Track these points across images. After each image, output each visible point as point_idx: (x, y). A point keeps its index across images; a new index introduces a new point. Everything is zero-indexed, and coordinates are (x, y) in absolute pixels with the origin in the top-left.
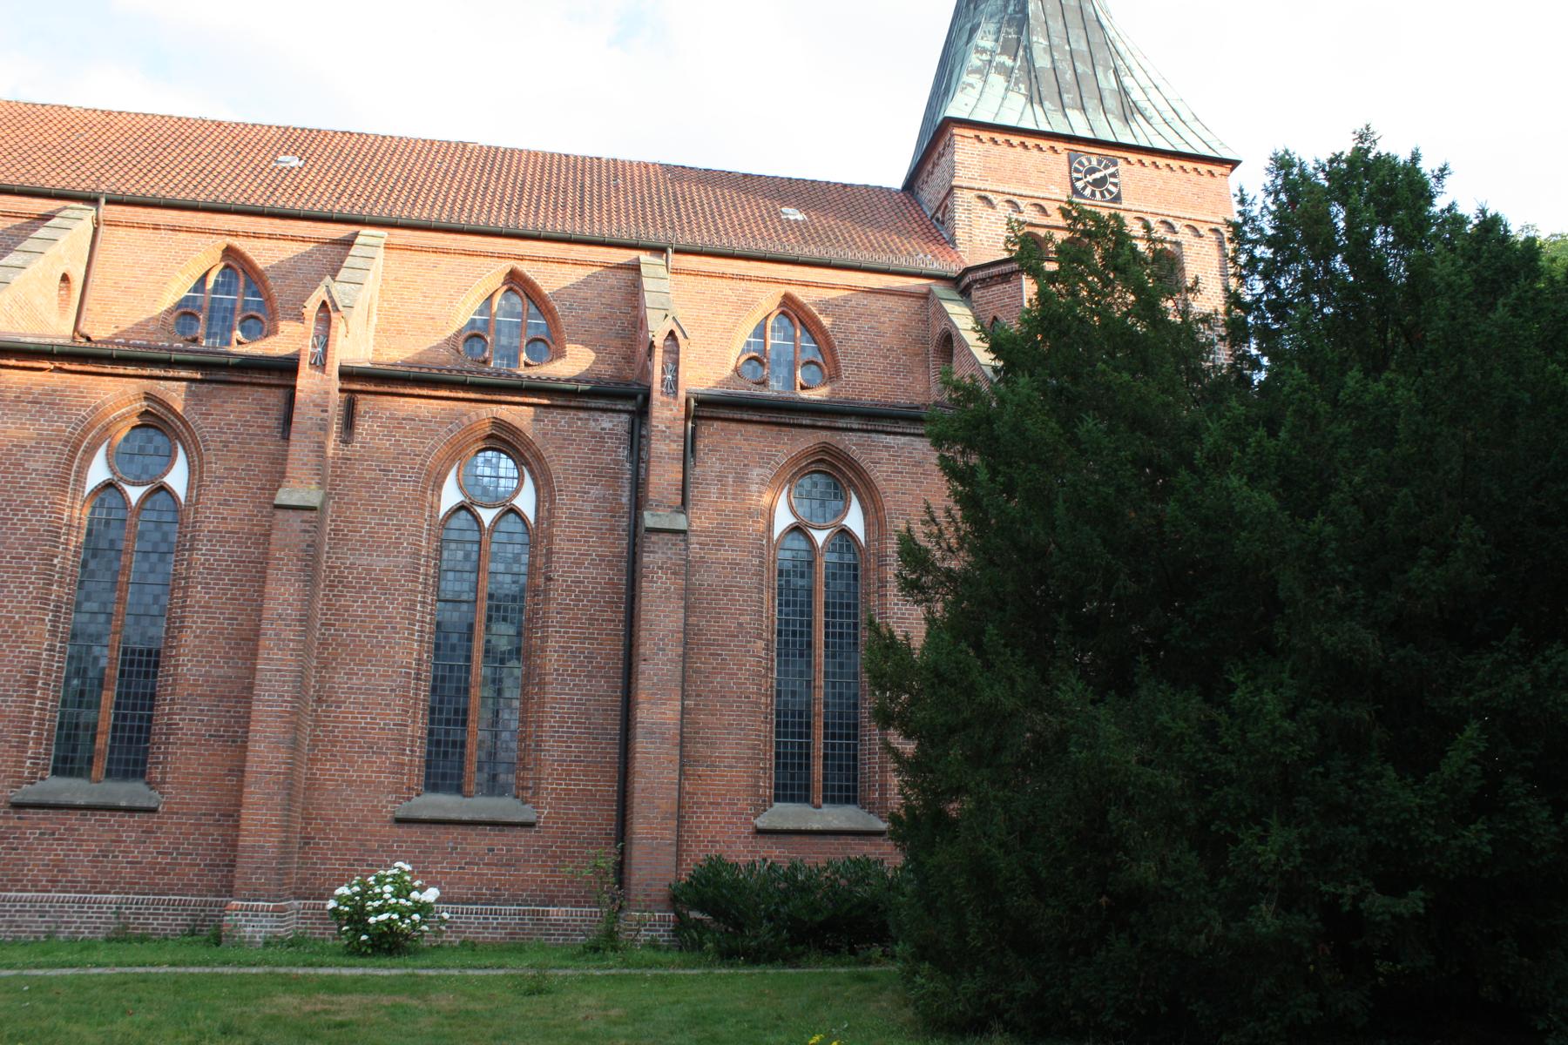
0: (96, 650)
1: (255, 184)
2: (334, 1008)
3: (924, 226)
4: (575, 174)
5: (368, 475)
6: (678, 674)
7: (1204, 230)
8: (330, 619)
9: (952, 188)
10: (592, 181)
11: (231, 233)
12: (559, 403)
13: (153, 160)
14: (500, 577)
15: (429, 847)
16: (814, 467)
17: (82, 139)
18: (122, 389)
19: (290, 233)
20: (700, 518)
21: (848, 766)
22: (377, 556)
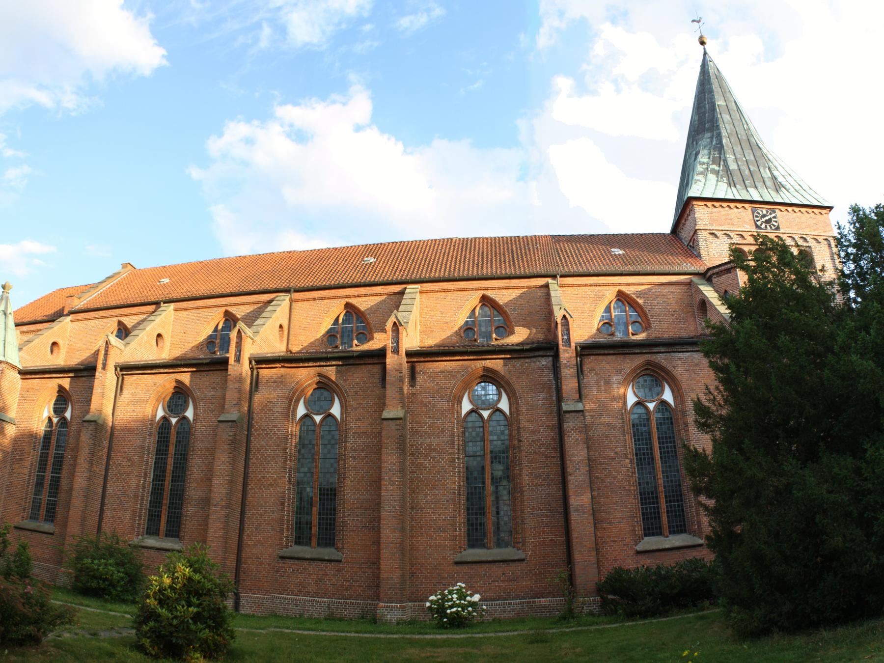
0: (308, 489)
1: (355, 273)
4: (508, 245)
5: (425, 400)
6: (588, 481)
7: (821, 239)
9: (696, 231)
11: (347, 297)
12: (515, 356)
14: (495, 443)
16: (644, 373)
18: (307, 373)
19: (374, 292)
21: (680, 515)
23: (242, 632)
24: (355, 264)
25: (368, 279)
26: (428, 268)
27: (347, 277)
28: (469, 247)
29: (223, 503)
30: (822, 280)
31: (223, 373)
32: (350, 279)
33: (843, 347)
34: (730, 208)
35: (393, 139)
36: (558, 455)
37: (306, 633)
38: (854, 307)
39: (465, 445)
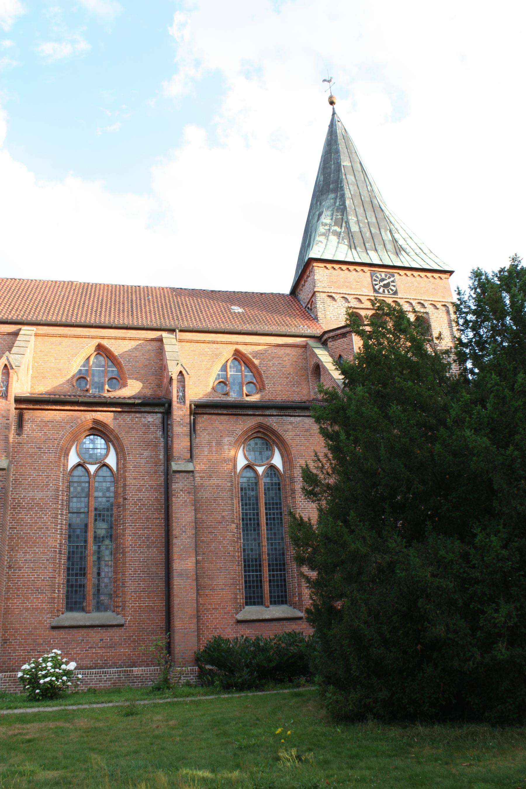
2: (25, 731)
3: (302, 312)
4: (128, 294)
5: (31, 451)
7: (439, 305)
8: (14, 525)
9: (315, 292)
10: (136, 298)
12: (126, 410)
14: (100, 499)
15: (69, 641)
16: (255, 435)
21: (281, 585)
22: (37, 492)
26: (45, 310)
28: (89, 292)
30: (438, 348)
33: (456, 421)
34: (349, 270)
38: (471, 378)
39: (69, 501)
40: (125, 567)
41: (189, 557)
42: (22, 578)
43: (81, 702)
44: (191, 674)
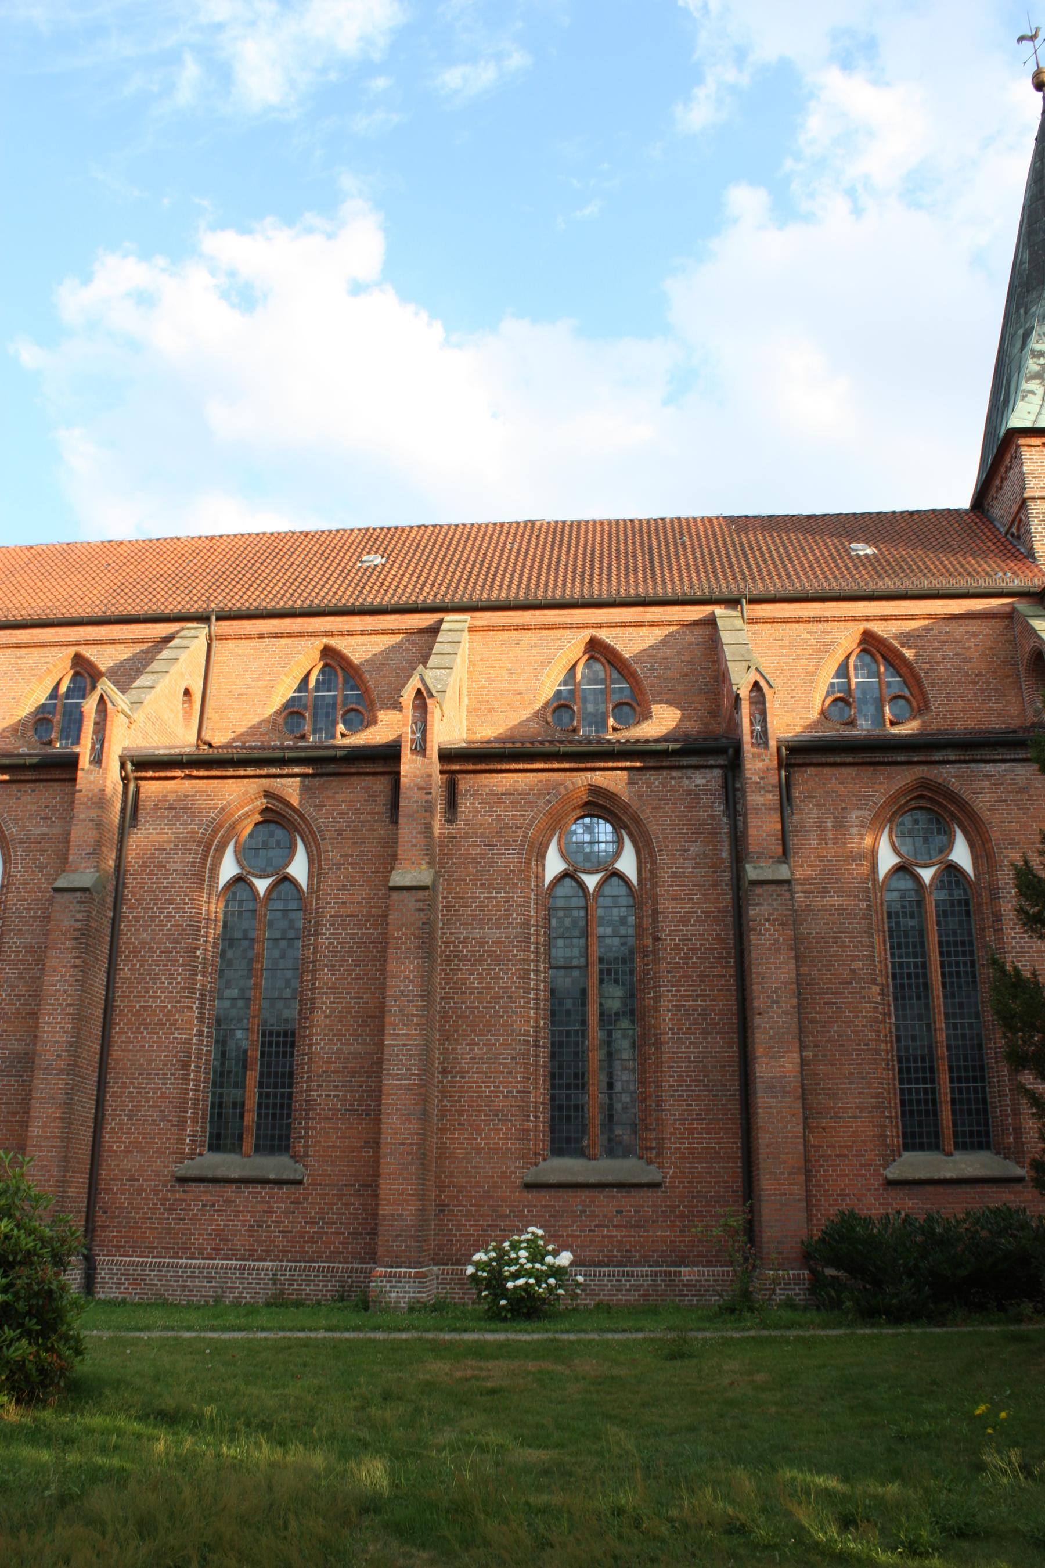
0: (239, 1034)
1: (344, 585)
2: (484, 1374)
3: (999, 544)
4: (642, 536)
5: (474, 851)
9: (1024, 501)
10: (659, 542)
12: (651, 764)
13: (253, 575)
14: (608, 941)
15: (558, 1211)
16: (913, 804)
17: (191, 565)
18: (243, 790)
19: (380, 627)
20: (802, 866)
21: (978, 1111)
23: (100, 1338)
24: (344, 568)
25: (369, 600)
26: (485, 580)
27: (327, 594)
28: (566, 539)
29: (62, 1065)
31: (67, 787)
32: (333, 597)
35: (424, 316)
36: (732, 971)
37: (227, 1335)
40: (661, 1072)
41: (786, 1052)
42: (467, 1092)
43: (584, 1327)
44: (795, 1284)
